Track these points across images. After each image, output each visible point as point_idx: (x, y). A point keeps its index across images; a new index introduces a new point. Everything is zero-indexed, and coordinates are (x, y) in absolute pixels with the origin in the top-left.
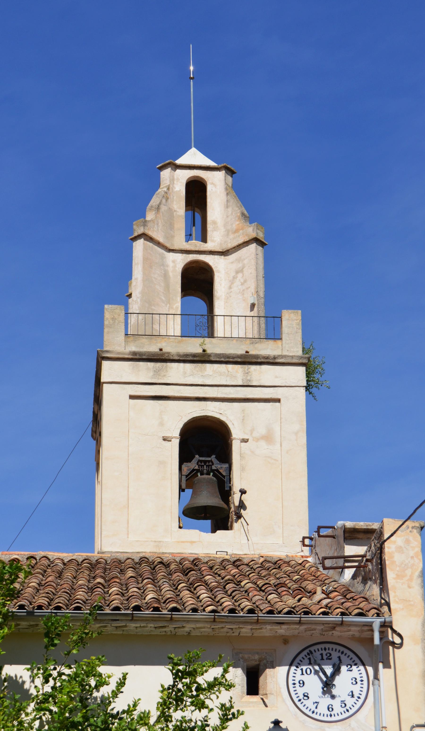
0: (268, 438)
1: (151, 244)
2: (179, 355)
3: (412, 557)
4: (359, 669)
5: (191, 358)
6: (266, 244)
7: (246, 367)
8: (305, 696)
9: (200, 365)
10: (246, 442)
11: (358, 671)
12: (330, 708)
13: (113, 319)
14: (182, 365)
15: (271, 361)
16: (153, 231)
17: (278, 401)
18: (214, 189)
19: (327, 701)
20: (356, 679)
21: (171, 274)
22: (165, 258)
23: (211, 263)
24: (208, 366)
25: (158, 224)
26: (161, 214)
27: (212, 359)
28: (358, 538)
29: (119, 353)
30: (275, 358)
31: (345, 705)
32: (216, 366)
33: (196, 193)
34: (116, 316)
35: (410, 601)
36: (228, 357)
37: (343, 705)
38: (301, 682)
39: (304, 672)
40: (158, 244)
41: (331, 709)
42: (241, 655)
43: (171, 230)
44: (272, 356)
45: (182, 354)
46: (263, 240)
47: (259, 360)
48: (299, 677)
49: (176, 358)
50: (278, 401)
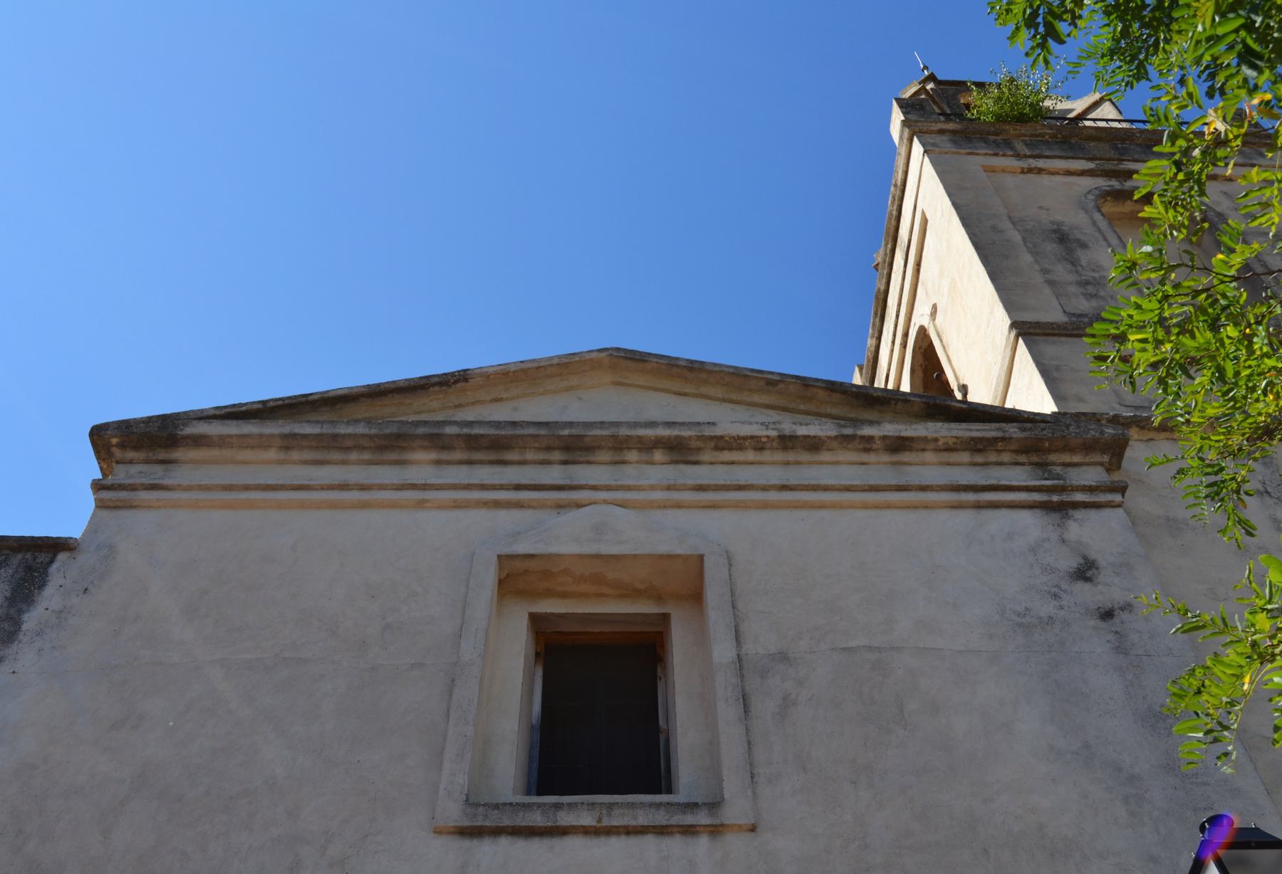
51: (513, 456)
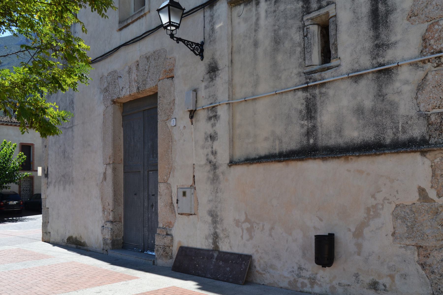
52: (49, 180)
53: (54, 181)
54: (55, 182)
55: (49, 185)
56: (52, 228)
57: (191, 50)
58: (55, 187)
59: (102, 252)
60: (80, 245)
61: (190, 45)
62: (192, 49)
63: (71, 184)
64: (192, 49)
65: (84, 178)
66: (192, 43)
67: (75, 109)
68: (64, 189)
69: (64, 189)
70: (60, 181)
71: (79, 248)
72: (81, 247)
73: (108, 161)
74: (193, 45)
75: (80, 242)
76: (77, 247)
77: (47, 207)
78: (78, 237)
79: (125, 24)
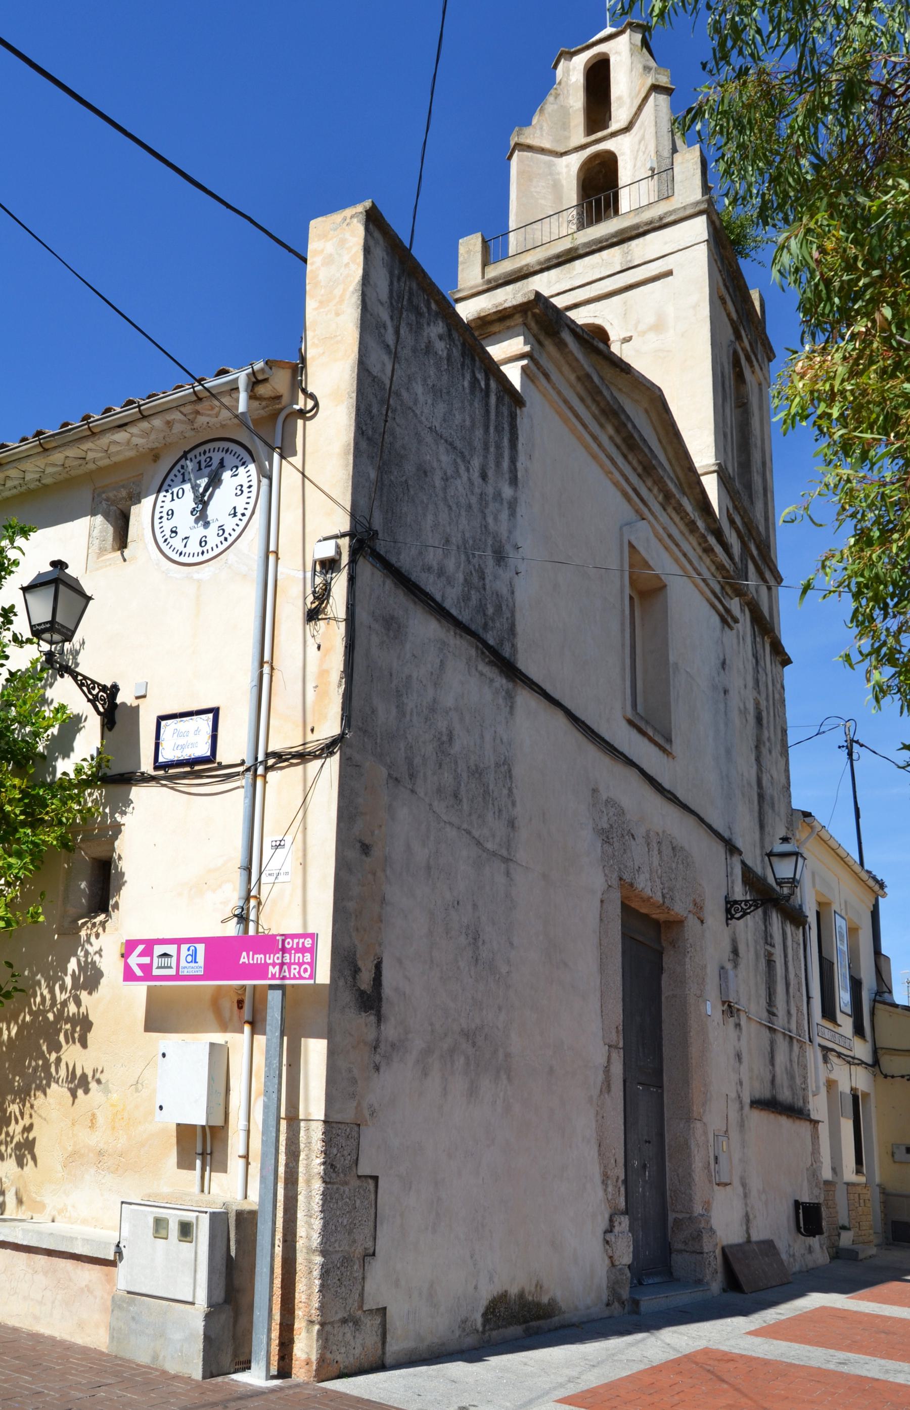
0: (658, 327)
1: (529, 154)
2: (540, 263)
3: (347, 265)
4: (247, 469)
5: (555, 261)
6: (672, 90)
7: (625, 245)
8: (172, 532)
9: (567, 265)
10: (629, 341)
11: (248, 473)
12: (203, 542)
13: (469, 252)
14: (546, 274)
15: (657, 225)
16: (534, 137)
17: (669, 273)
18: (618, 58)
19: (200, 531)
20: (242, 486)
21: (564, 182)
22: (554, 165)
23: (613, 149)
24: (578, 263)
25: (541, 128)
26: (547, 115)
27: (581, 252)
28: (495, 333)
29: (471, 288)
30: (661, 219)
31: (224, 530)
32: (587, 259)
33: (598, 77)
34: (471, 248)
35: (336, 336)
36: (601, 242)
37: (221, 532)
38: (170, 512)
39: (175, 497)
40: (542, 151)
41: (203, 544)
42: (104, 496)
43: (565, 130)
44: (657, 217)
45: (542, 260)
46: (669, 86)
47: (641, 230)
48: (168, 505)
49: (538, 268)
50: (669, 273)
51: (615, 407)
52: (390, 1031)
53: (418, 1043)
54: (427, 1052)
55: (387, 1058)
56: (397, 1284)
57: (89, 700)
58: (425, 1074)
59: (607, 1313)
60: (539, 1318)
61: (88, 686)
62: (91, 697)
63: (504, 1077)
64: (91, 697)
65: (551, 1071)
66: (93, 682)
67: (518, 804)
68: (472, 1092)
69: (472, 1092)
70: (452, 1051)
71: (538, 1332)
72: (541, 1323)
73: (614, 1036)
74: (94, 688)
75: (538, 1305)
76: (526, 1330)
77: (364, 1169)
78: (529, 1288)
79: (642, 725)
